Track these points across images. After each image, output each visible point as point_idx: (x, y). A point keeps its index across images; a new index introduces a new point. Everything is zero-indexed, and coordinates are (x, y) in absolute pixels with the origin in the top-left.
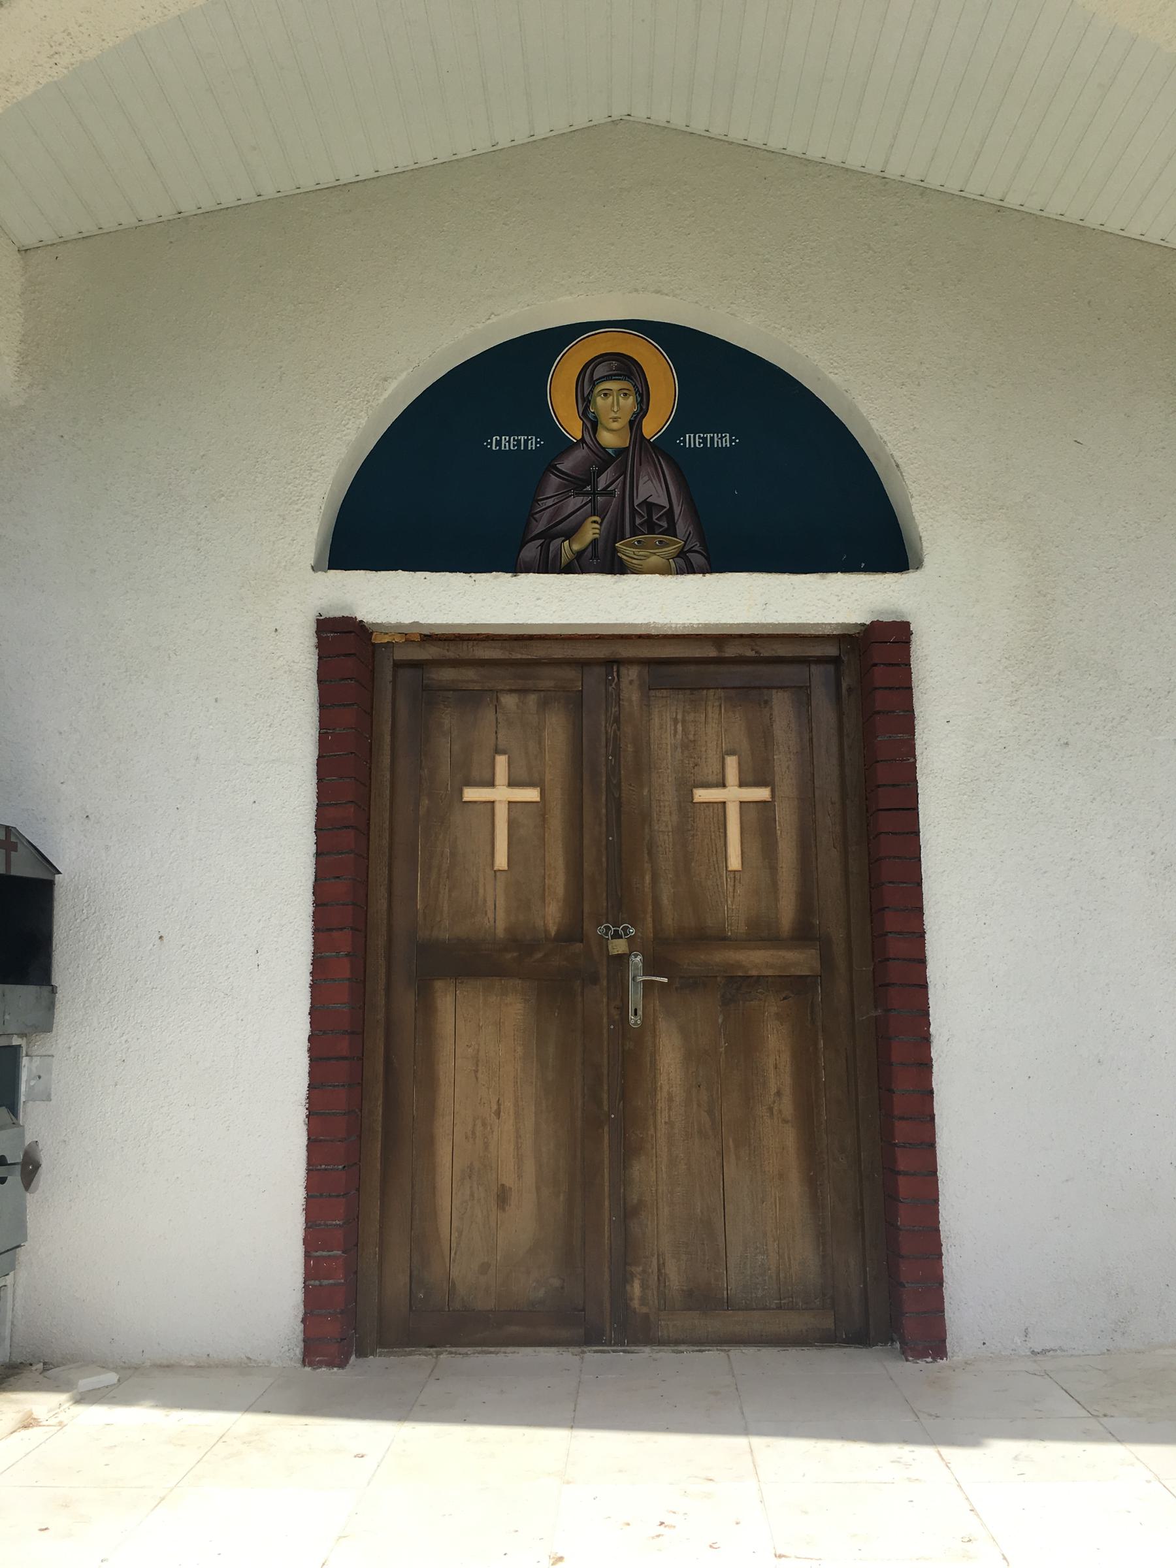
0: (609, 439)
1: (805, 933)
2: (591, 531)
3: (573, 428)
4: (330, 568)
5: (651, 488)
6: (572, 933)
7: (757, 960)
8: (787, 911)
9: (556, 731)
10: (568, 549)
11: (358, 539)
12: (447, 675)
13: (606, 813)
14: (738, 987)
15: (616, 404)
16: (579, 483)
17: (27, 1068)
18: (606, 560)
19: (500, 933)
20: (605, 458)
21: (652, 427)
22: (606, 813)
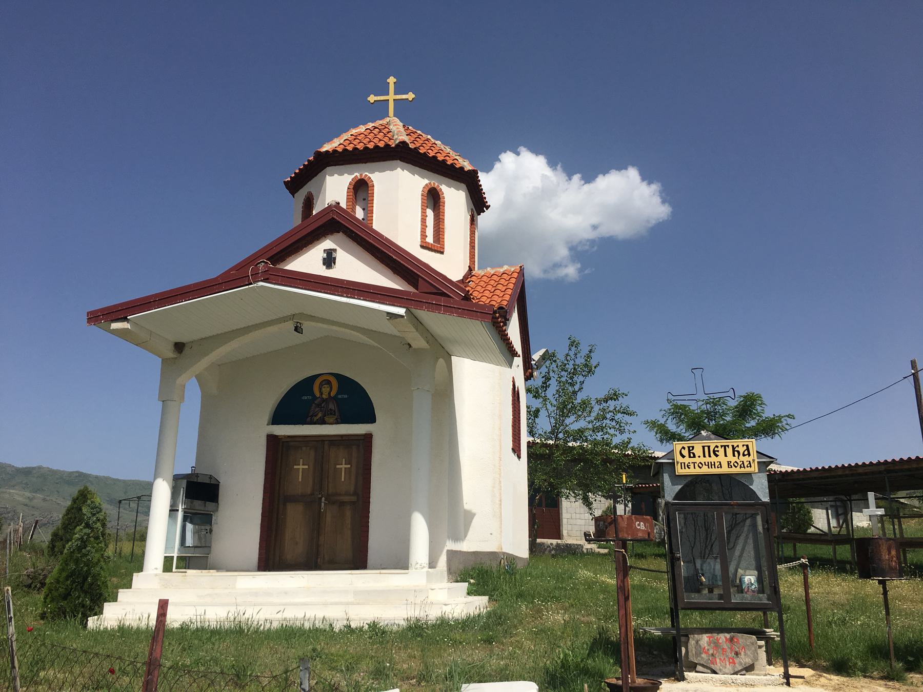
0: (324, 396)
1: (355, 493)
2: (320, 415)
3: (318, 395)
4: (217, 502)
5: (332, 406)
6: (312, 494)
7: (346, 499)
8: (352, 489)
9: (312, 453)
10: (315, 419)
11: (278, 418)
12: (292, 444)
13: (321, 471)
14: (342, 504)
15: (326, 389)
16: (318, 405)
17: (214, 518)
18: (322, 422)
19: (655, 187)
20: (323, 400)
21: (332, 394)
22: (321, 471)
